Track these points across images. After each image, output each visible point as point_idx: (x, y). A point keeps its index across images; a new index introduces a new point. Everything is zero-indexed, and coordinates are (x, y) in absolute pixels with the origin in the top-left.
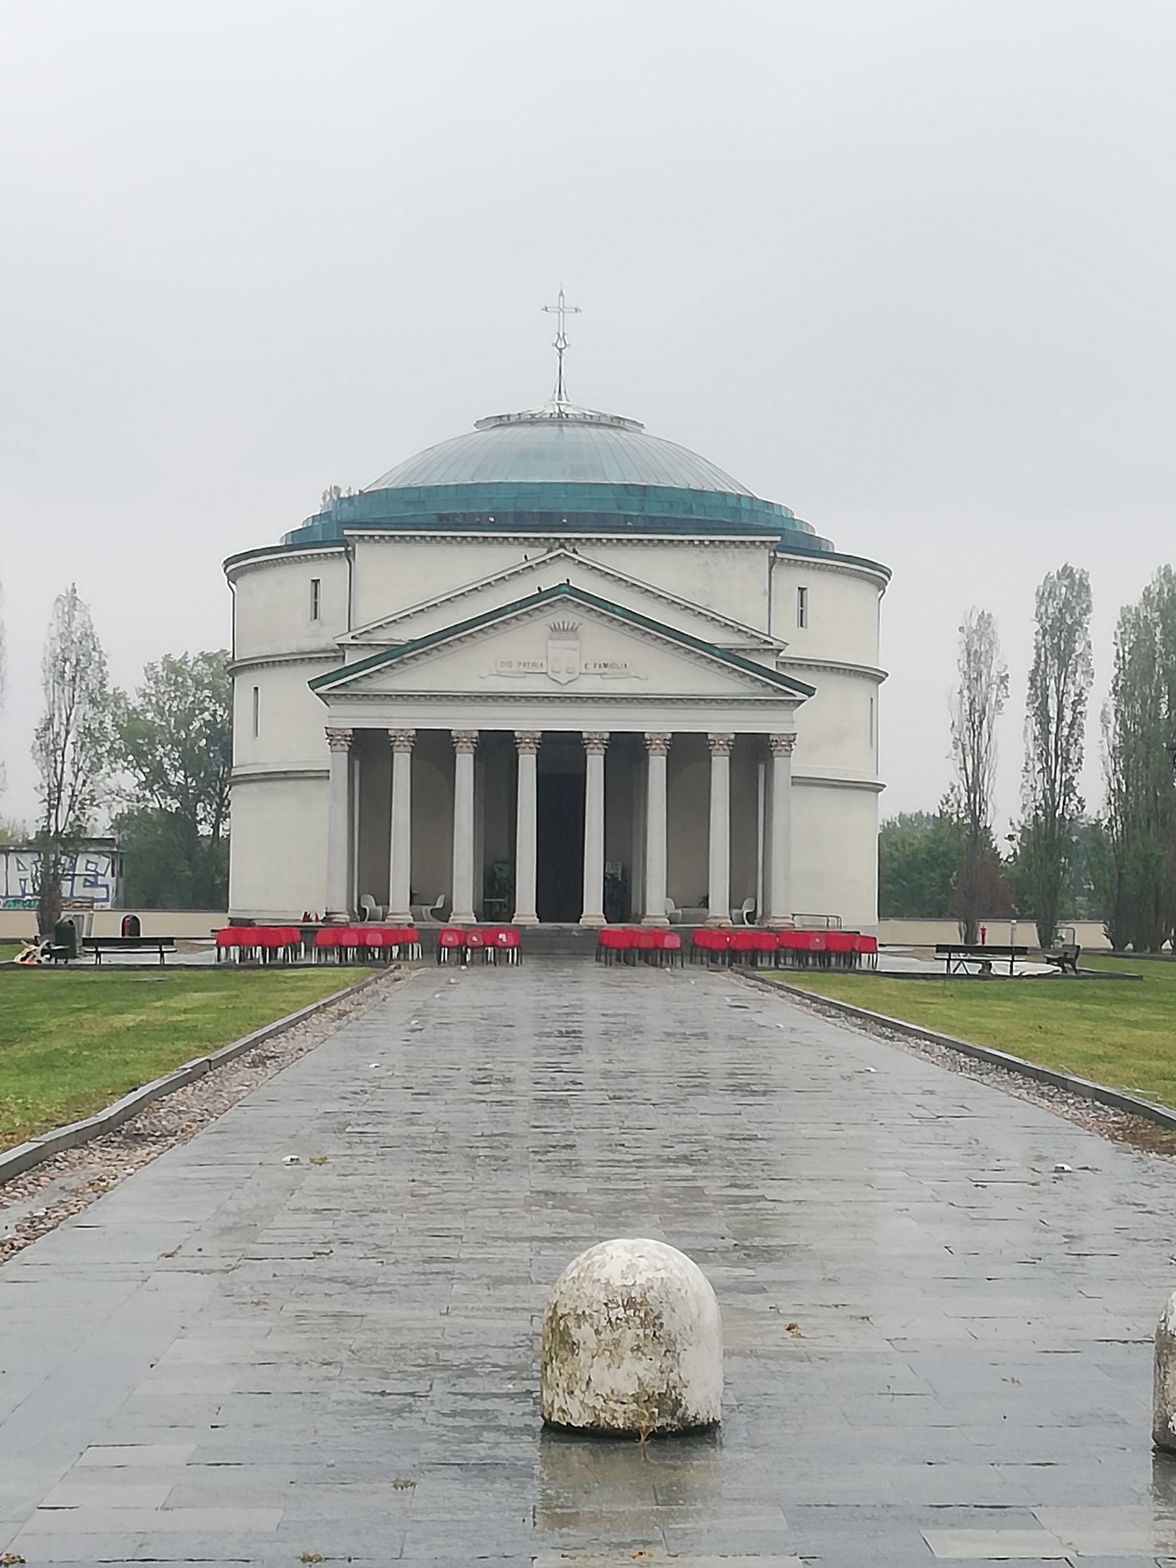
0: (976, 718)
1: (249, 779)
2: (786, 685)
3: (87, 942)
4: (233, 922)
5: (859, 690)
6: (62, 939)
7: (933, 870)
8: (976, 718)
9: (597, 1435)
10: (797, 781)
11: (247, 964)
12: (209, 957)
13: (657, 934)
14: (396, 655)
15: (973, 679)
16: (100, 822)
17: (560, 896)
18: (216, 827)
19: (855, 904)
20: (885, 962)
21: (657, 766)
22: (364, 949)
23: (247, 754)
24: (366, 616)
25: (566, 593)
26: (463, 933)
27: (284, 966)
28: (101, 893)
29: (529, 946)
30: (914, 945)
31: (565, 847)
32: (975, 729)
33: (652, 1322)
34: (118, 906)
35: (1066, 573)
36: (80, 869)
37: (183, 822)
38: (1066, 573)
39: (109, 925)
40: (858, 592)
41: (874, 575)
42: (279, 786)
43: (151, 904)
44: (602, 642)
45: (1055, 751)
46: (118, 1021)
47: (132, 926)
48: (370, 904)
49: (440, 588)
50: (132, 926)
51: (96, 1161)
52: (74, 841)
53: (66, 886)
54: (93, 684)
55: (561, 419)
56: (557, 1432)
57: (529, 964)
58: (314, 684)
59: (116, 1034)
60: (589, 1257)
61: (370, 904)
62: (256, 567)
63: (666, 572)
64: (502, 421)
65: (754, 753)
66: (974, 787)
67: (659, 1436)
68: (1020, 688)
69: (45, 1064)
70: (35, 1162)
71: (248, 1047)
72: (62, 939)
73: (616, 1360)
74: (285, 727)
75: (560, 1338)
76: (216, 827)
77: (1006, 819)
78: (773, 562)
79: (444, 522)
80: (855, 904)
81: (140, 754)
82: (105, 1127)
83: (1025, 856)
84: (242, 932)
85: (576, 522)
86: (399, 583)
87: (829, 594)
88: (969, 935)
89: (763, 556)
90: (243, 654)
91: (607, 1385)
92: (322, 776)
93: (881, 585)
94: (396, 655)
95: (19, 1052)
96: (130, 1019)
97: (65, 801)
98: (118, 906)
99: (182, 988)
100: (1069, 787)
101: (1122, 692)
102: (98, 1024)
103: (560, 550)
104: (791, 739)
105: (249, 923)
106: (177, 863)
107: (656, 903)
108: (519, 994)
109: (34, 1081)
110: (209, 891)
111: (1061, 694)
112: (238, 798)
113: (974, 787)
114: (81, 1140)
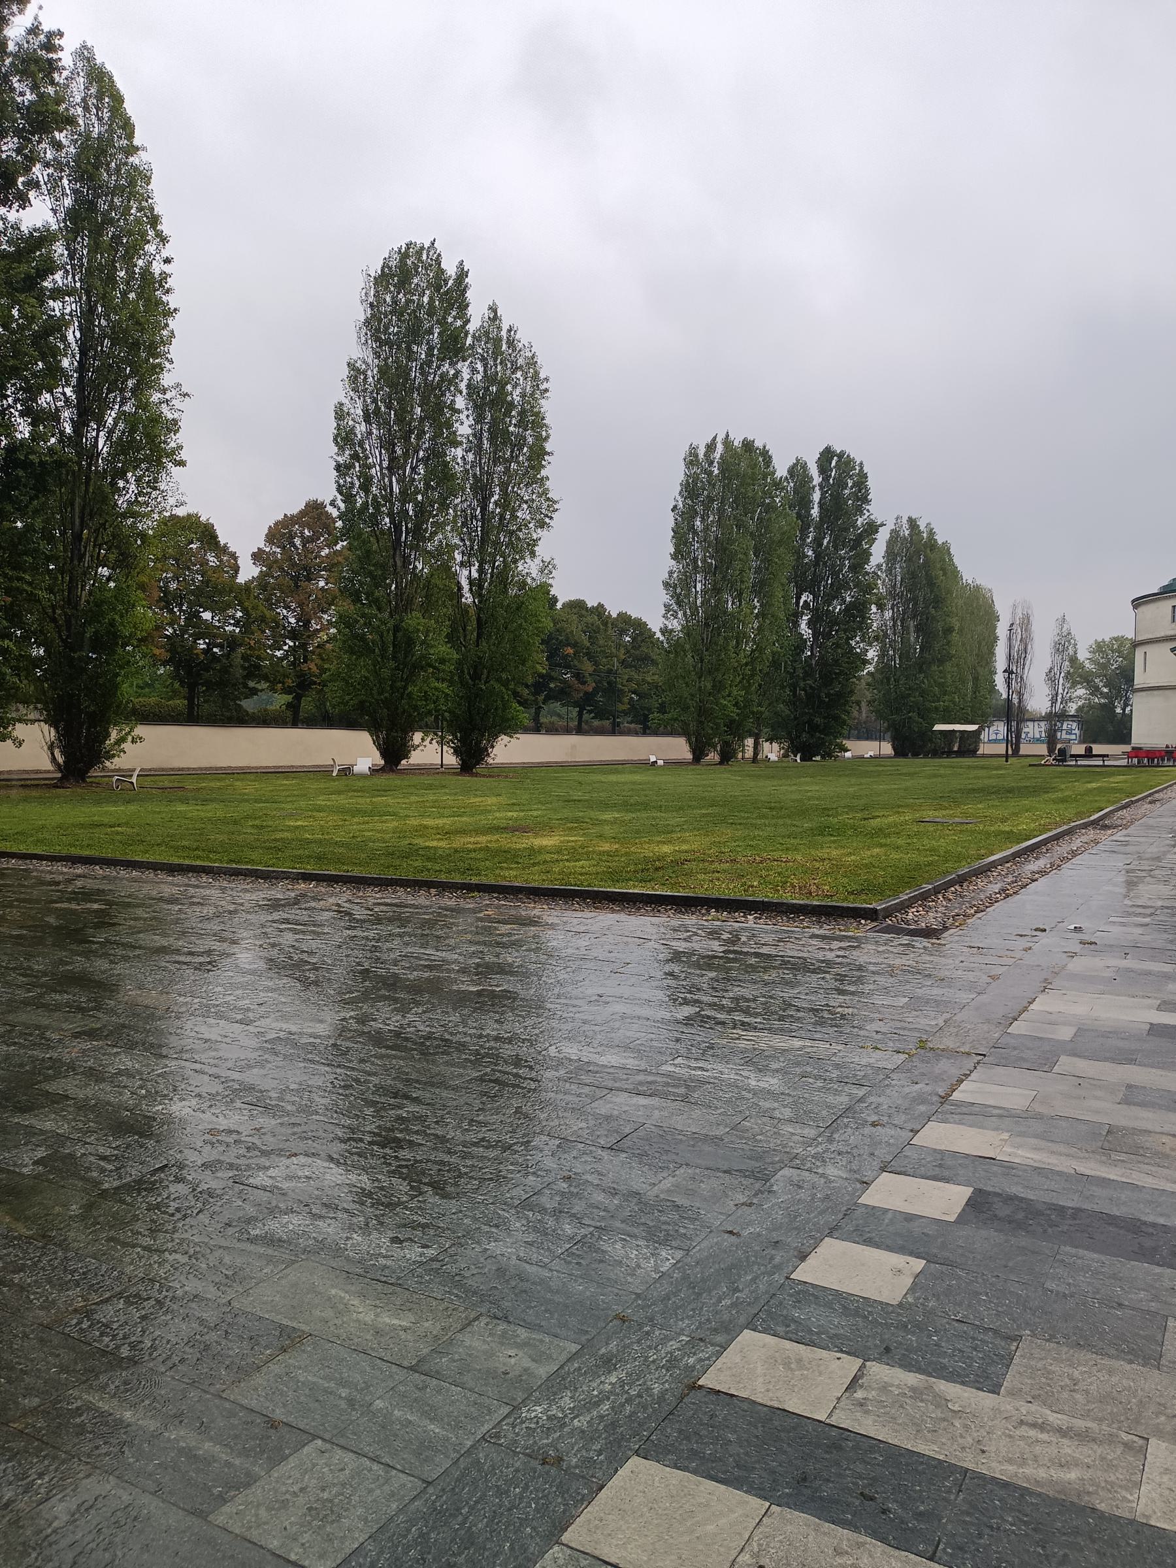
3: (1072, 756)
4: (1133, 748)
12: (1124, 762)
16: (1072, 708)
18: (1124, 710)
23: (1139, 680)
27: (1158, 766)
28: (1074, 737)
36: (1065, 727)
37: (1108, 708)
39: (1079, 749)
42: (1155, 692)
43: (1094, 742)
46: (1089, 786)
50: (1089, 750)
51: (1091, 834)
52: (1063, 716)
53: (1059, 734)
54: (1071, 652)
59: (1090, 791)
60: (860, 1545)
69: (1063, 800)
70: (1069, 832)
71: (1147, 797)
76: (1124, 710)
81: (1088, 682)
82: (1093, 823)
84: (1137, 752)
90: (1140, 638)
96: (1094, 785)
97: (1059, 700)
99: (1113, 774)
102: (1080, 787)
105: (1140, 749)
106: (1108, 725)
109: (1061, 806)
114: (1085, 826)
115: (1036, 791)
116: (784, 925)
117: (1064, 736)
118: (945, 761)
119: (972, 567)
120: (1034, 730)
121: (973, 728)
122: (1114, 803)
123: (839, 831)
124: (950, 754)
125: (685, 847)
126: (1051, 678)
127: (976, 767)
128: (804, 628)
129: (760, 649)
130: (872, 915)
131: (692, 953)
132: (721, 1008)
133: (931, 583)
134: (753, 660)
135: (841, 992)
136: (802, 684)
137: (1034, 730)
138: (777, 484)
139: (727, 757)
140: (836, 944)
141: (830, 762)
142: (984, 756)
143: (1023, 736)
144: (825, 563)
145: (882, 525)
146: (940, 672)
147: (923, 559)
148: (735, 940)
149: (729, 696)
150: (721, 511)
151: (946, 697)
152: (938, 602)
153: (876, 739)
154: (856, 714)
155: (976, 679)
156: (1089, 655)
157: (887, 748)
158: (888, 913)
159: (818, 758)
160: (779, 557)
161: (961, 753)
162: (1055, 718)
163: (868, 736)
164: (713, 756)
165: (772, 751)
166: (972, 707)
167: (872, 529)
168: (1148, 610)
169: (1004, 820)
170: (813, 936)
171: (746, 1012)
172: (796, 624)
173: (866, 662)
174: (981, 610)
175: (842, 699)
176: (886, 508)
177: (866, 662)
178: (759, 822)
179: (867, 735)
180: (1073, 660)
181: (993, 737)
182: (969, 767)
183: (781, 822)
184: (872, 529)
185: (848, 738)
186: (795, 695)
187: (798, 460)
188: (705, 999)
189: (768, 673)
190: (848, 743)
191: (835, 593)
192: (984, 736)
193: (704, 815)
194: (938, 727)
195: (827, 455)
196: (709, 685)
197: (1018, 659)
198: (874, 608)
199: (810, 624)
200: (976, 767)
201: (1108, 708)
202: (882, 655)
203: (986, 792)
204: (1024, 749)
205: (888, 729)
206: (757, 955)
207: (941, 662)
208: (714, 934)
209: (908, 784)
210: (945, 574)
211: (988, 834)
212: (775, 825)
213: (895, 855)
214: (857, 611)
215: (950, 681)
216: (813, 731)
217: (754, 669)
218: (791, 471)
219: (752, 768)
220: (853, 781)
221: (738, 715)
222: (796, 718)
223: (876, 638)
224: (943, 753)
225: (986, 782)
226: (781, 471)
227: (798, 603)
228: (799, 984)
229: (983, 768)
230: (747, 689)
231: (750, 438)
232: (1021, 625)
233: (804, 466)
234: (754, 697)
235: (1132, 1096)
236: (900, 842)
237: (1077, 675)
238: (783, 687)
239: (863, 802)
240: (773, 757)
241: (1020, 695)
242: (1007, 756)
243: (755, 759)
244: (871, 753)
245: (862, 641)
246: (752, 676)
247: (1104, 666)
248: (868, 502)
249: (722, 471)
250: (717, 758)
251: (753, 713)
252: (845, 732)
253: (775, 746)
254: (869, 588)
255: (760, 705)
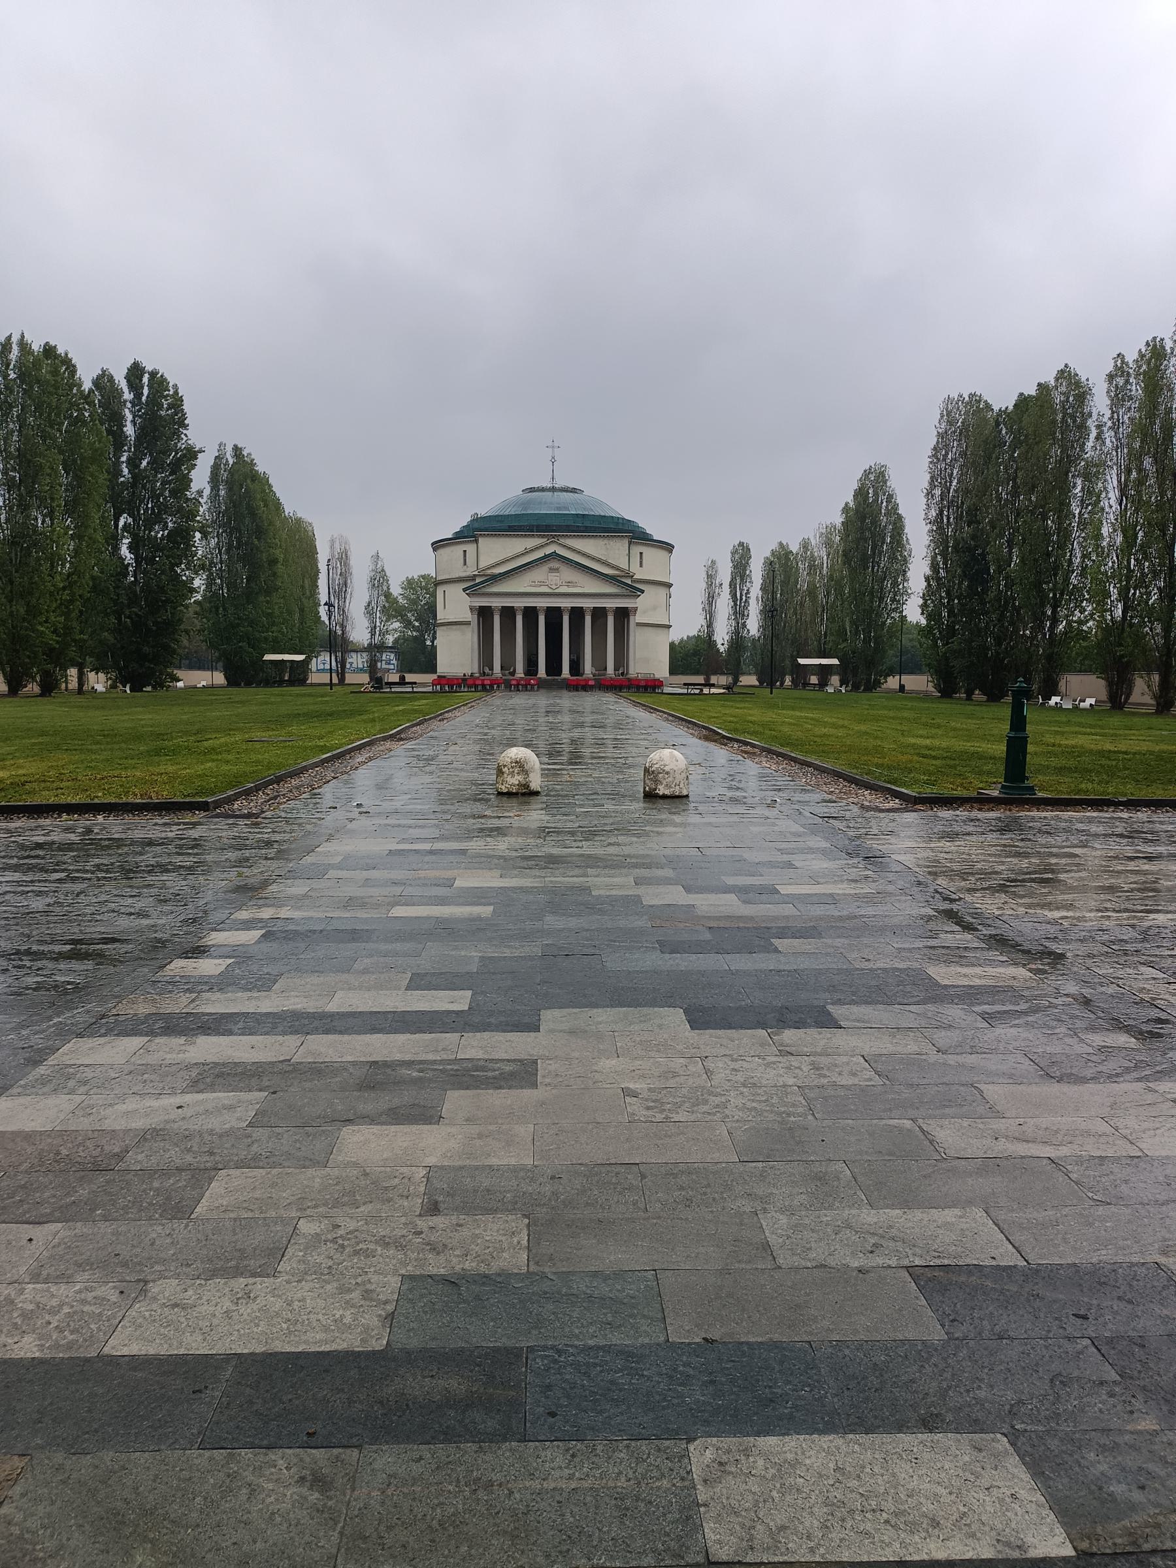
0: (711, 599)
1: (443, 624)
2: (633, 589)
3: (387, 683)
5: (662, 591)
6: (378, 682)
7: (693, 657)
8: (711, 599)
9: (509, 794)
10: (638, 624)
11: (442, 691)
12: (430, 689)
13: (587, 680)
14: (495, 579)
15: (710, 585)
16: (390, 640)
17: (554, 666)
19: (661, 670)
20: (667, 690)
21: (588, 620)
22: (483, 685)
23: (441, 616)
24: (482, 565)
25: (554, 556)
26: (518, 681)
29: (542, 685)
30: (675, 685)
31: (558, 648)
32: (710, 604)
33: (522, 766)
34: (398, 671)
35: (741, 544)
37: (420, 640)
38: (741, 544)
39: (394, 678)
40: (661, 554)
41: (668, 547)
43: (410, 672)
44: (568, 574)
45: (739, 612)
47: (402, 678)
48: (487, 670)
49: (510, 553)
50: (402, 678)
51: (388, 744)
52: (381, 647)
55: (553, 489)
56: (500, 794)
57: (542, 691)
58: (464, 590)
61: (487, 670)
62: (443, 546)
63: (591, 546)
64: (532, 490)
65: (623, 615)
66: (710, 625)
67: (523, 794)
68: (726, 589)
70: (370, 744)
72: (378, 682)
73: (513, 776)
74: (455, 605)
75: (500, 772)
77: (722, 637)
78: (630, 543)
79: (511, 529)
80: (661, 670)
83: (729, 651)
84: (441, 680)
85: (559, 528)
86: (494, 552)
87: (652, 555)
88: (707, 679)
89: (626, 542)
91: (512, 781)
92: (468, 623)
93: (671, 551)
94: (495, 579)
95: (365, 717)
96: (401, 708)
98: (398, 671)
100: (744, 625)
101: (763, 589)
102: (389, 709)
103: (553, 540)
104: (636, 609)
106: (418, 655)
107: (588, 668)
108: (541, 700)
109: (370, 725)
110: (431, 667)
111: (741, 590)
112: (440, 632)
113: (710, 625)
115: (351, 714)
116: (128, 819)
117: (384, 666)
118: (276, 690)
119: (294, 497)
120: (357, 660)
121: (301, 657)
122: (409, 721)
123: (174, 752)
124: (281, 683)
125: (21, 772)
126: (369, 610)
127: (304, 695)
128: (124, 551)
129: (75, 571)
130: (204, 807)
131: (53, 843)
132: (87, 871)
133: (253, 513)
134: (71, 585)
135: (178, 854)
136: (127, 612)
137: (357, 660)
138: (87, 398)
139: (49, 687)
140: (174, 828)
141: (161, 693)
142: (312, 685)
143: (348, 666)
144: (144, 487)
145: (201, 451)
146: (268, 602)
147: (243, 484)
148: (89, 831)
149: (46, 622)
150: (21, 420)
151: (275, 628)
152: (260, 532)
153: (208, 669)
154: (185, 642)
155: (302, 610)
156: (401, 591)
157: (219, 678)
158: (218, 804)
159: (149, 689)
160: (92, 476)
161: (292, 683)
162: (376, 649)
163: (200, 665)
164: (33, 688)
165: (98, 682)
166: (300, 638)
167: (191, 455)
168: (443, 552)
169: (321, 738)
170: (156, 824)
171: (107, 871)
172: (116, 548)
173: (193, 590)
174: (302, 541)
175: (170, 627)
176: (207, 433)
177: (193, 590)
178: (94, 747)
179: (199, 664)
180: (388, 595)
181: (321, 667)
182: (298, 695)
183: (116, 746)
184: (191, 455)
185: (180, 668)
186: (120, 620)
187: (104, 371)
188: (71, 868)
189: (88, 599)
190: (179, 673)
191: (156, 518)
192: (313, 665)
193: (35, 744)
194: (267, 657)
195: (135, 372)
196: (22, 611)
197: (341, 590)
198: (198, 535)
199: (131, 548)
200: (304, 695)
201: (420, 640)
202: (210, 582)
203: (309, 716)
204: (350, 678)
205: (219, 660)
206: (109, 839)
207: (268, 593)
208: (68, 830)
209: (240, 710)
210: (266, 505)
211: (306, 748)
212: (112, 750)
213: (225, 767)
214: (181, 537)
215: (277, 612)
216: (142, 661)
217: (72, 594)
218: (97, 382)
219: (80, 699)
220: (186, 709)
221: (58, 642)
222: (123, 647)
223: (203, 567)
224: (275, 682)
225: (311, 707)
226: (87, 385)
227: (116, 526)
228: (147, 852)
229: (310, 695)
230: (67, 615)
231: (52, 343)
232: (340, 559)
233: (111, 379)
234: (75, 624)
235: (367, 882)
236: (230, 757)
237: (392, 609)
238: (107, 615)
239: (196, 727)
240: (100, 688)
241: (343, 627)
242: (331, 684)
243: (80, 691)
244: (204, 683)
245: (188, 569)
246: (71, 601)
247: (414, 602)
248: (186, 426)
249: (22, 376)
250: (37, 689)
251: (75, 641)
252: (177, 662)
253: (101, 676)
254: (192, 514)
255: (82, 632)
